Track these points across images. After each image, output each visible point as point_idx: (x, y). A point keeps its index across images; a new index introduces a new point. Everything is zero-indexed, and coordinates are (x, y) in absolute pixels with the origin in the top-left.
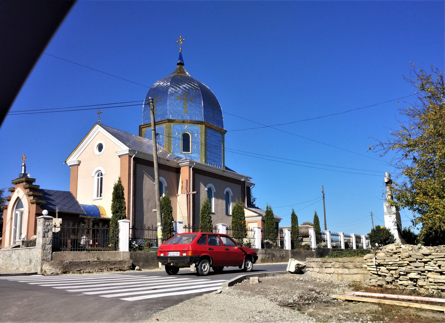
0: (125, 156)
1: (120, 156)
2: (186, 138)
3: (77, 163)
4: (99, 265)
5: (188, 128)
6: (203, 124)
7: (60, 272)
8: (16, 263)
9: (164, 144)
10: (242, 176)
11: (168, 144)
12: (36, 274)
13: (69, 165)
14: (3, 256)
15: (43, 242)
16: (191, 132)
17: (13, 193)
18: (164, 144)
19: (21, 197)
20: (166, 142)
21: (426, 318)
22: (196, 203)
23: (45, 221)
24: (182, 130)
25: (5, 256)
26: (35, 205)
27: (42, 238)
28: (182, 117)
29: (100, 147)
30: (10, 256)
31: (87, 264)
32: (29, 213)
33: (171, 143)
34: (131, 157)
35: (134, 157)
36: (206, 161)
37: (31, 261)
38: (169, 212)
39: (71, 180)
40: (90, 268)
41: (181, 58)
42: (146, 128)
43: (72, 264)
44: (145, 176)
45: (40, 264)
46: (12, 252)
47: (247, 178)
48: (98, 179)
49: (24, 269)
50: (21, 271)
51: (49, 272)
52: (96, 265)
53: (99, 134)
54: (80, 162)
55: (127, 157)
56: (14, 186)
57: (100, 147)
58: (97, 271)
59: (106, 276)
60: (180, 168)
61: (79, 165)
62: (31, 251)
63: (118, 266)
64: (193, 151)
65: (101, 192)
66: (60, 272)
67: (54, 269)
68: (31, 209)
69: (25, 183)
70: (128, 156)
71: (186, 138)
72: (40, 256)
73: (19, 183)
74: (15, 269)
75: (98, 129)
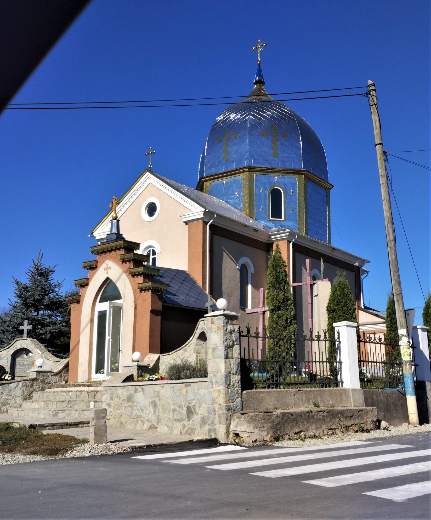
0: (196, 222)
1: (186, 223)
2: (276, 196)
4: (328, 420)
5: (279, 180)
6: (302, 174)
7: (268, 438)
8: (149, 414)
9: (242, 206)
10: (357, 258)
11: (249, 206)
12: (213, 443)
13: (97, 238)
14: (112, 399)
15: (226, 368)
16: (283, 186)
17: (92, 271)
18: (242, 206)
19: (113, 278)
20: (245, 202)
22: (297, 301)
23: (227, 323)
24: (270, 183)
25: (116, 400)
26: (149, 293)
27: (223, 360)
28: (270, 163)
29: (152, 209)
30: (130, 399)
31: (309, 417)
32: (136, 308)
33: (253, 205)
34: (205, 223)
35: (211, 224)
36: (306, 233)
37: (190, 412)
38: (352, 311)
40: (314, 426)
41: (260, 73)
42: (210, 182)
43: (286, 418)
44: (225, 254)
45: (223, 420)
46: (136, 391)
47: (363, 262)
49: (171, 428)
50: (177, 435)
51: (247, 439)
52: (324, 420)
53: (150, 187)
55: (200, 224)
56: (97, 258)
57: (152, 209)
58: (326, 433)
59: (353, 443)
60: (273, 243)
62: (189, 389)
63: (357, 421)
64: (287, 217)
66: (268, 438)
67: (256, 431)
68: (140, 301)
69: (122, 252)
70: (201, 222)
71: (276, 196)
72: (221, 400)
73: (110, 251)
74: (146, 426)
75: (148, 179)
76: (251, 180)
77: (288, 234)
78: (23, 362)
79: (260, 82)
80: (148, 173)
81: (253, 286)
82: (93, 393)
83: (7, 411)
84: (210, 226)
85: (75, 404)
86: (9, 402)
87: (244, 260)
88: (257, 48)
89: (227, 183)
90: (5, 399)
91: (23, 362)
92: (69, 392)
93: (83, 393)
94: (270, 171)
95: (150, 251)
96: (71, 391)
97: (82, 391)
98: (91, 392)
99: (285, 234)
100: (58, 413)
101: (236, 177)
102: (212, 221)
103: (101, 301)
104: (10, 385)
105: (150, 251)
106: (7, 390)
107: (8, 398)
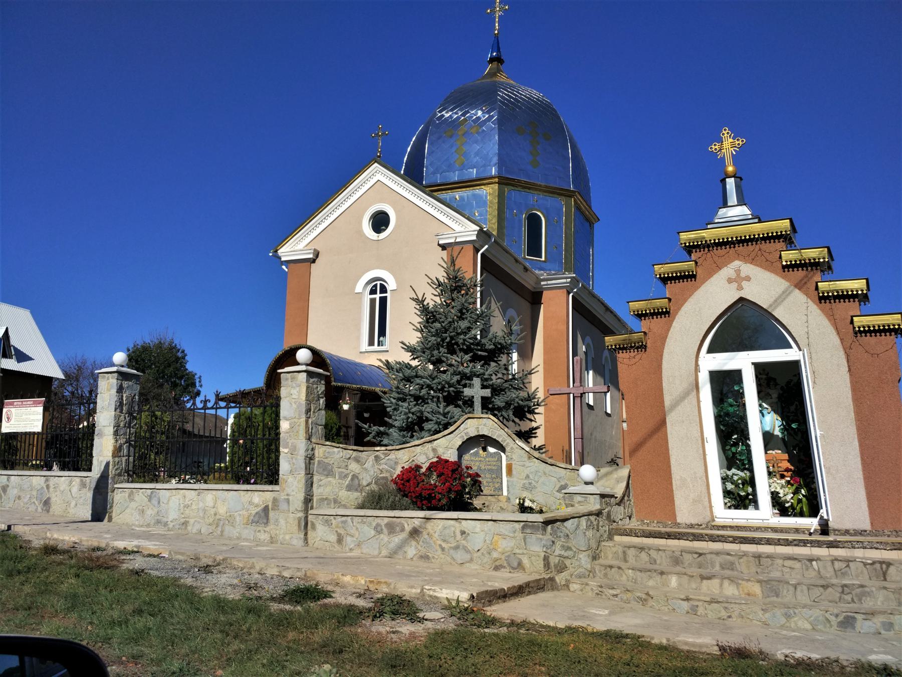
2: (534, 223)
3: (311, 256)
6: (571, 197)
21: (90, 432)
29: (380, 221)
34: (477, 251)
39: (289, 297)
48: (373, 301)
54: (317, 254)
55: (469, 249)
57: (380, 221)
61: (314, 261)
65: (382, 333)
76: (501, 196)
77: (569, 280)
78: (477, 464)
79: (498, 60)
80: (376, 164)
81: (520, 355)
82: (878, 566)
83: (567, 586)
84: (482, 255)
85: (864, 594)
86: (568, 562)
87: (511, 312)
88: (493, 12)
89: (462, 198)
90: (560, 556)
91: (477, 464)
92: (811, 560)
93: (851, 564)
94: (528, 187)
95: (376, 286)
96: (818, 559)
97: (848, 561)
98: (873, 563)
99: (564, 280)
100: (854, 618)
101: (478, 191)
102: (486, 247)
103: (711, 350)
104: (566, 524)
105: (376, 286)
106: (562, 535)
107: (566, 554)
